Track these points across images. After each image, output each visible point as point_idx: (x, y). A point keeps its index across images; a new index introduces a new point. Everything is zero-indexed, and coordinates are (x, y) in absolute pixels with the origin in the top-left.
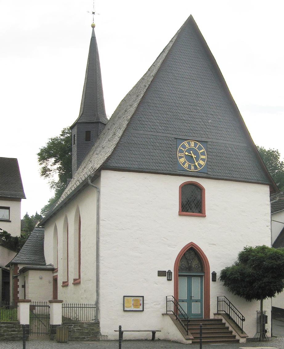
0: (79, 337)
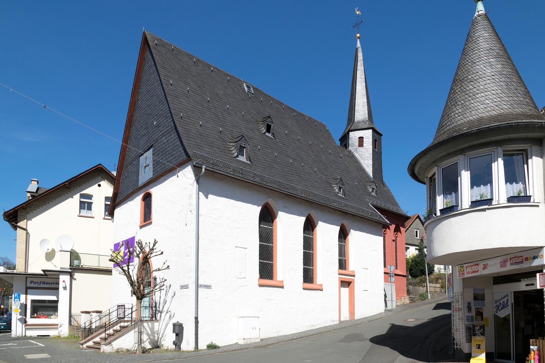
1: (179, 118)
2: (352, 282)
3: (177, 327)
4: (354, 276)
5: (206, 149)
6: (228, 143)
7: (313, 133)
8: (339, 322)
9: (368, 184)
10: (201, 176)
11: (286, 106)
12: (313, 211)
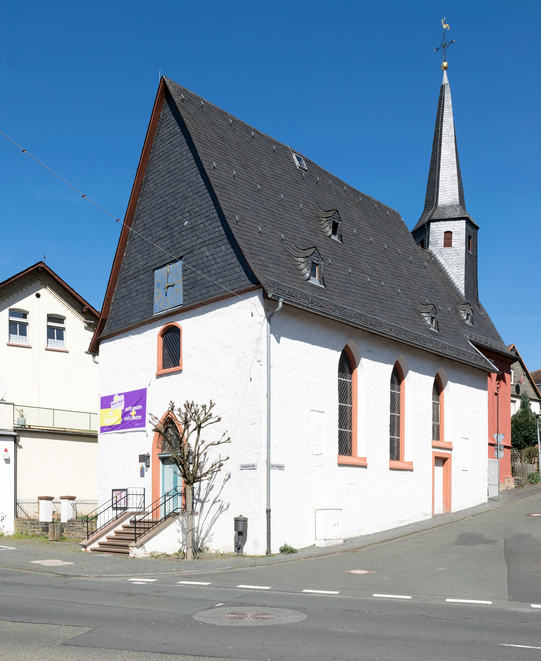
1: (233, 223)
2: (448, 458)
3: (241, 522)
4: (451, 449)
5: (273, 270)
6: (295, 258)
7: (385, 229)
8: (432, 517)
9: (460, 306)
10: (277, 312)
11: (349, 187)
12: (402, 355)
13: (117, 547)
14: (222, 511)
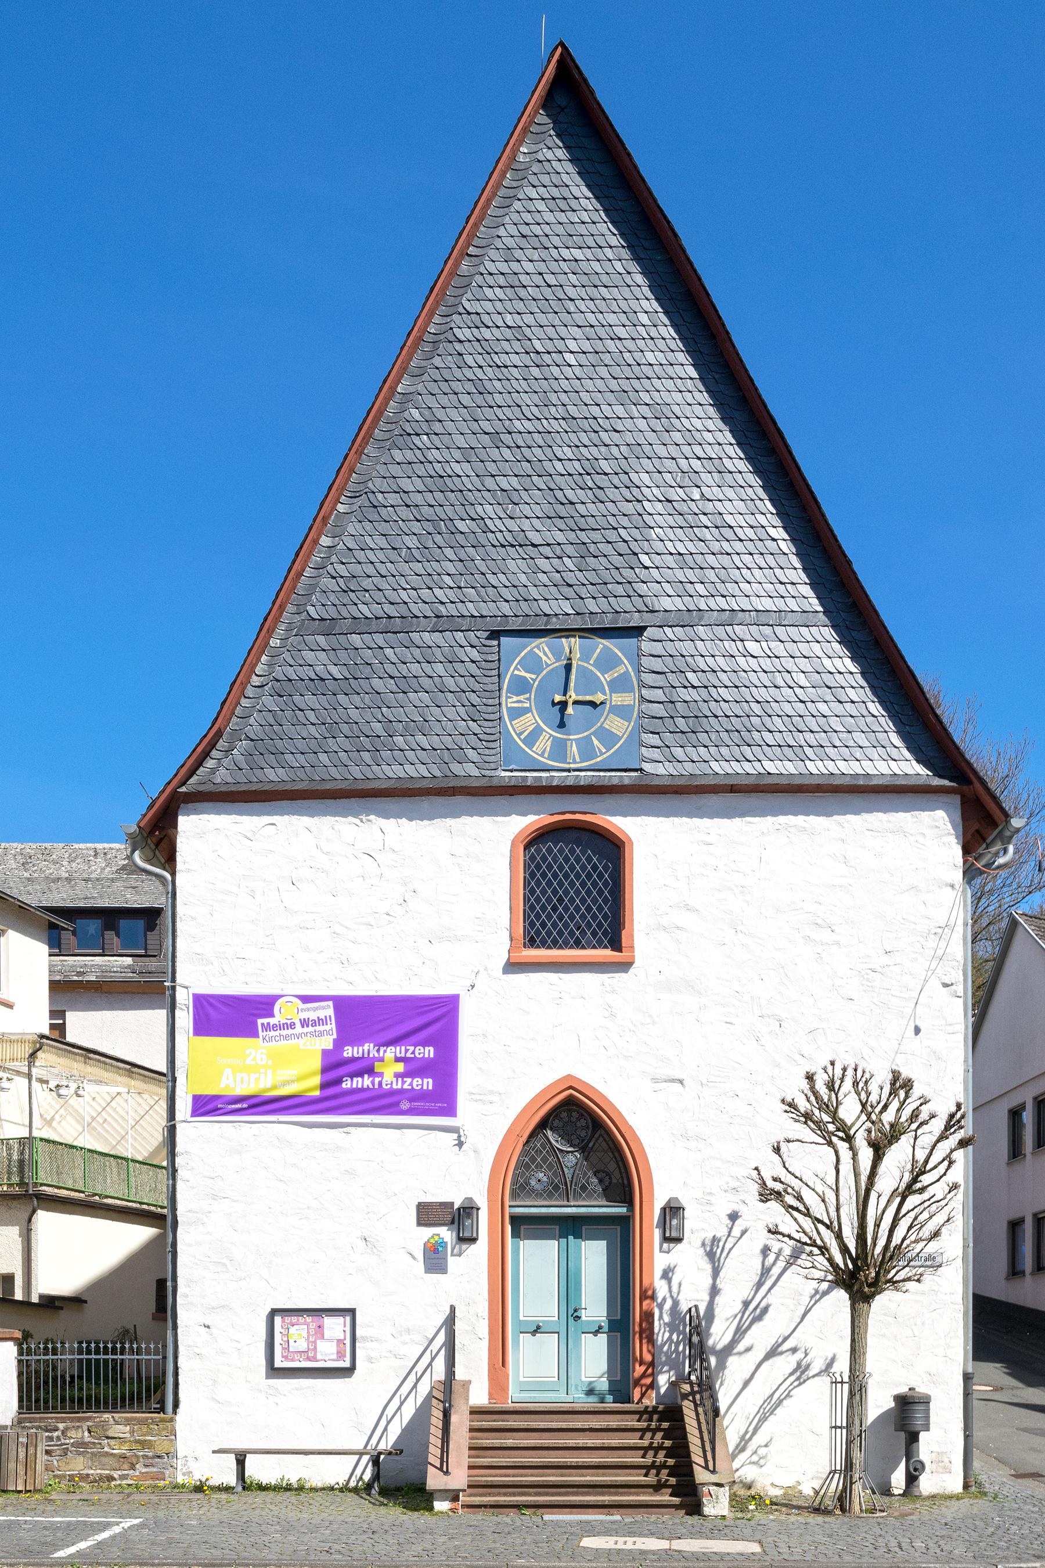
0: (88, 1475)
13: (558, 1490)
14: (804, 1377)
